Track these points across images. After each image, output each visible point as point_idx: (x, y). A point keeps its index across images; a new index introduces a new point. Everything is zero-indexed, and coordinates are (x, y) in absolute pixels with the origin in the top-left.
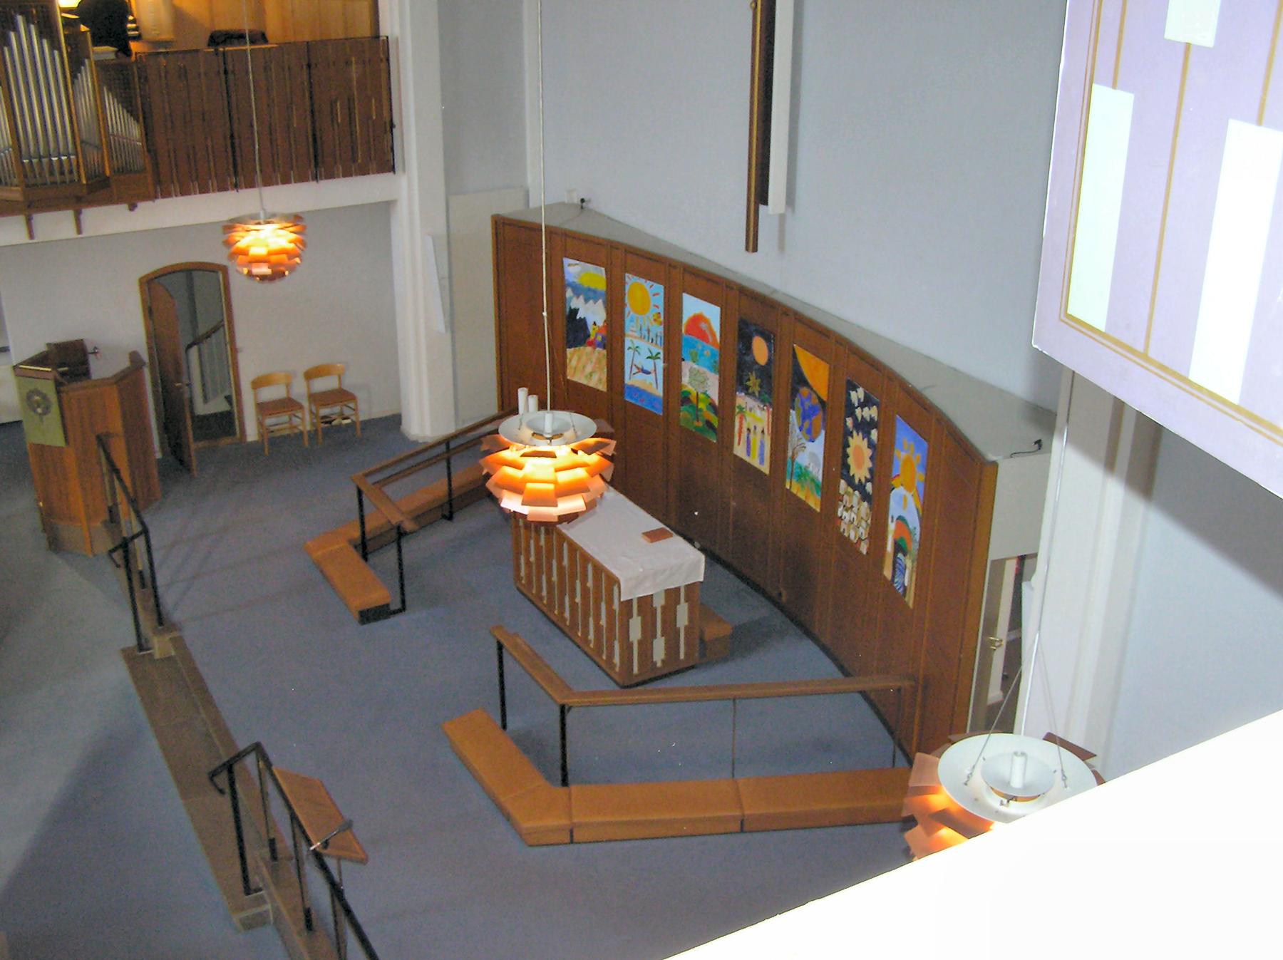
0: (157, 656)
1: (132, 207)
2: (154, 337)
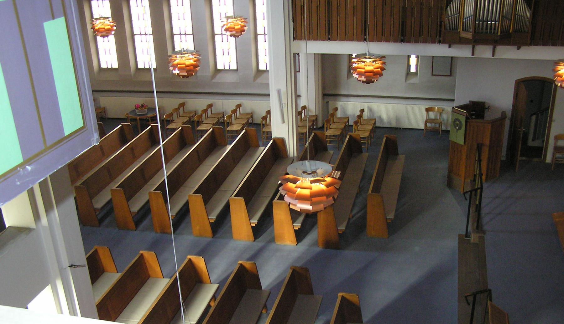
0: (472, 241)
1: (519, 48)
2: (515, 106)
